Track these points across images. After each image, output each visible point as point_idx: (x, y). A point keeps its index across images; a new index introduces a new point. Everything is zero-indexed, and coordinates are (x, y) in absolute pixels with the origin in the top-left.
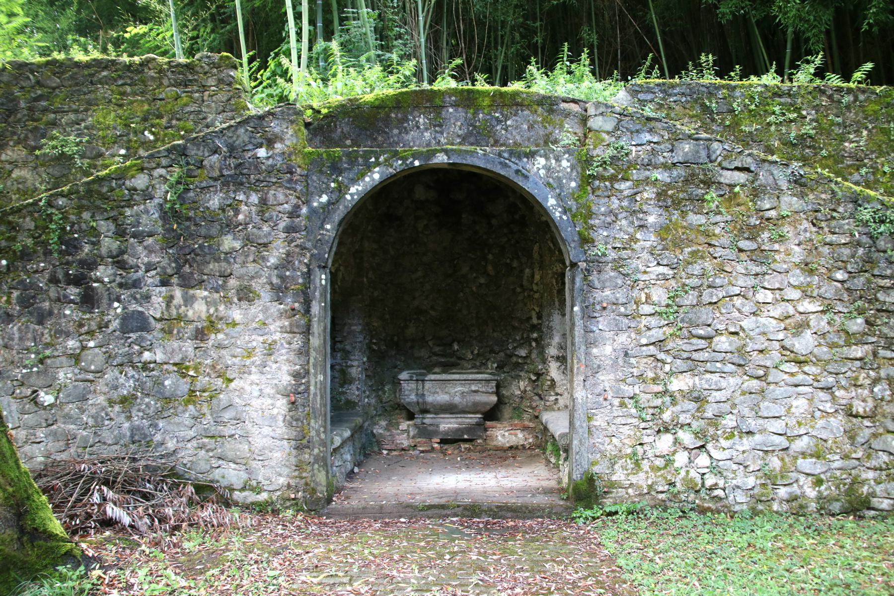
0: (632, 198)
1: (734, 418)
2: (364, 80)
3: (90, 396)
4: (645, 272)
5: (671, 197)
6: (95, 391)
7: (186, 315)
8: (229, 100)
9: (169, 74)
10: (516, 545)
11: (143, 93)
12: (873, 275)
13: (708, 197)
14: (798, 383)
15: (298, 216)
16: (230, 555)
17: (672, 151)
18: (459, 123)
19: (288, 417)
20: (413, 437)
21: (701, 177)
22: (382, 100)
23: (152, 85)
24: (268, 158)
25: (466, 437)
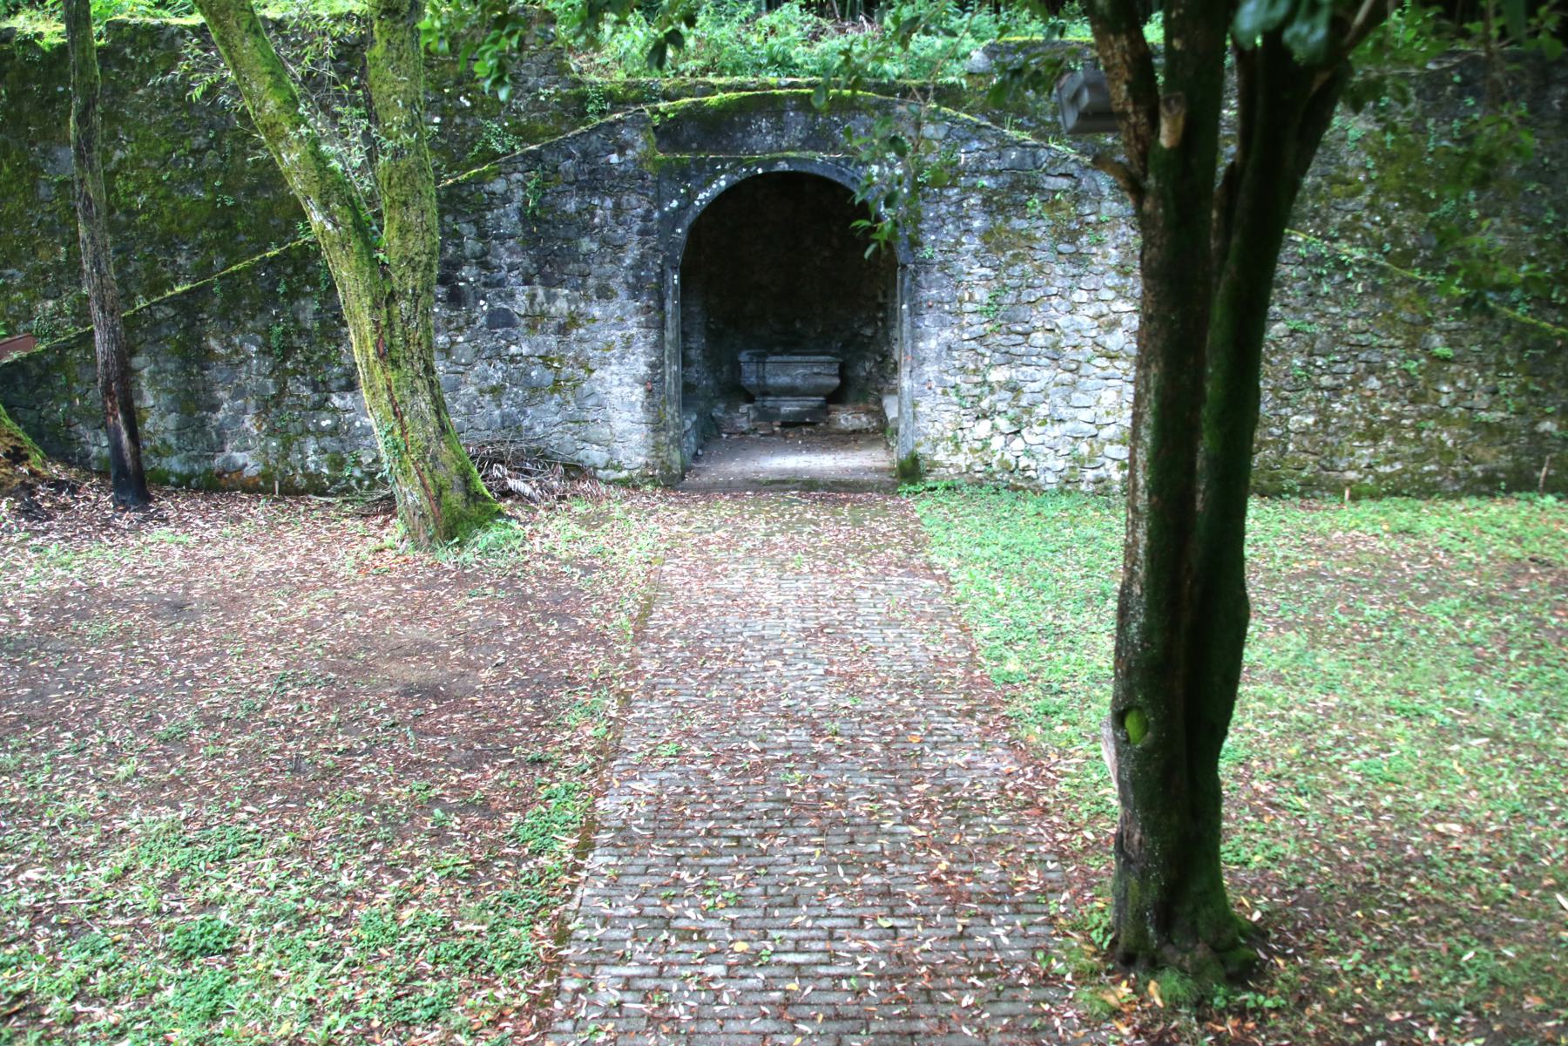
0: (959, 204)
10: (845, 510)
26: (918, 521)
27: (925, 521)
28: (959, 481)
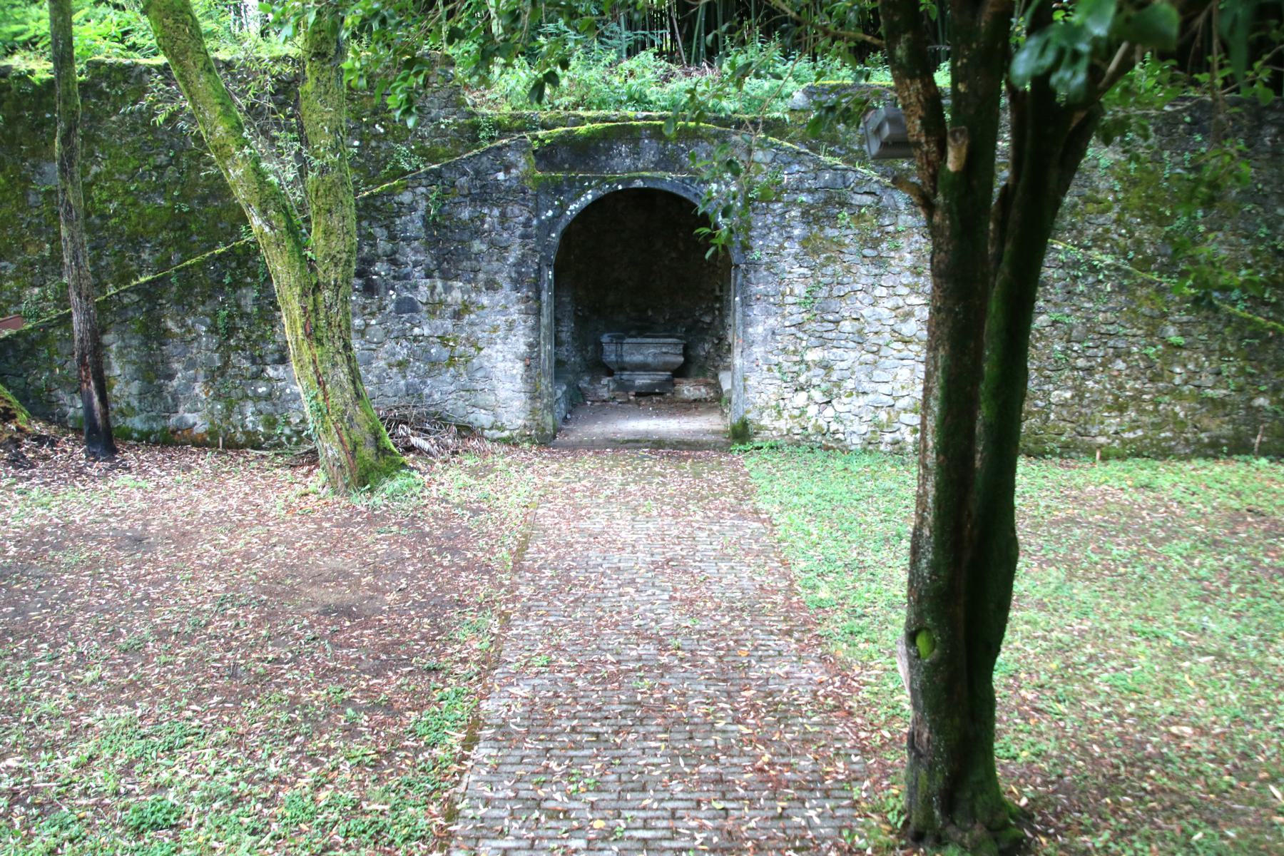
0: (782, 216)
26: (747, 474)
27: (753, 474)
28: (781, 442)
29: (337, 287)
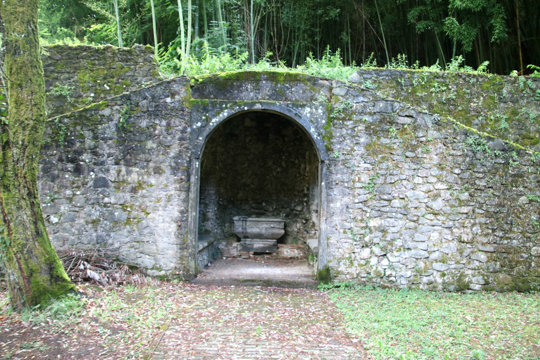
0: (353, 129)
1: (401, 241)
2: (221, 62)
3: (76, 219)
4: (358, 166)
5: (373, 129)
6: (79, 217)
7: (127, 180)
8: (150, 70)
9: (118, 55)
10: (289, 297)
11: (104, 65)
12: (474, 172)
13: (391, 130)
14: (433, 224)
15: (186, 133)
16: (148, 295)
17: (374, 106)
18: (268, 89)
19: (177, 233)
20: (240, 251)
21: (388, 120)
22: (230, 76)
23: (109, 61)
24: (171, 103)
25: (267, 251)
26: (333, 305)
27: (338, 305)
28: (352, 282)
29: (24, 147)
